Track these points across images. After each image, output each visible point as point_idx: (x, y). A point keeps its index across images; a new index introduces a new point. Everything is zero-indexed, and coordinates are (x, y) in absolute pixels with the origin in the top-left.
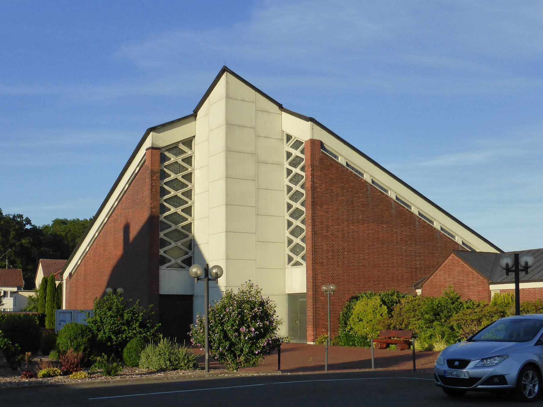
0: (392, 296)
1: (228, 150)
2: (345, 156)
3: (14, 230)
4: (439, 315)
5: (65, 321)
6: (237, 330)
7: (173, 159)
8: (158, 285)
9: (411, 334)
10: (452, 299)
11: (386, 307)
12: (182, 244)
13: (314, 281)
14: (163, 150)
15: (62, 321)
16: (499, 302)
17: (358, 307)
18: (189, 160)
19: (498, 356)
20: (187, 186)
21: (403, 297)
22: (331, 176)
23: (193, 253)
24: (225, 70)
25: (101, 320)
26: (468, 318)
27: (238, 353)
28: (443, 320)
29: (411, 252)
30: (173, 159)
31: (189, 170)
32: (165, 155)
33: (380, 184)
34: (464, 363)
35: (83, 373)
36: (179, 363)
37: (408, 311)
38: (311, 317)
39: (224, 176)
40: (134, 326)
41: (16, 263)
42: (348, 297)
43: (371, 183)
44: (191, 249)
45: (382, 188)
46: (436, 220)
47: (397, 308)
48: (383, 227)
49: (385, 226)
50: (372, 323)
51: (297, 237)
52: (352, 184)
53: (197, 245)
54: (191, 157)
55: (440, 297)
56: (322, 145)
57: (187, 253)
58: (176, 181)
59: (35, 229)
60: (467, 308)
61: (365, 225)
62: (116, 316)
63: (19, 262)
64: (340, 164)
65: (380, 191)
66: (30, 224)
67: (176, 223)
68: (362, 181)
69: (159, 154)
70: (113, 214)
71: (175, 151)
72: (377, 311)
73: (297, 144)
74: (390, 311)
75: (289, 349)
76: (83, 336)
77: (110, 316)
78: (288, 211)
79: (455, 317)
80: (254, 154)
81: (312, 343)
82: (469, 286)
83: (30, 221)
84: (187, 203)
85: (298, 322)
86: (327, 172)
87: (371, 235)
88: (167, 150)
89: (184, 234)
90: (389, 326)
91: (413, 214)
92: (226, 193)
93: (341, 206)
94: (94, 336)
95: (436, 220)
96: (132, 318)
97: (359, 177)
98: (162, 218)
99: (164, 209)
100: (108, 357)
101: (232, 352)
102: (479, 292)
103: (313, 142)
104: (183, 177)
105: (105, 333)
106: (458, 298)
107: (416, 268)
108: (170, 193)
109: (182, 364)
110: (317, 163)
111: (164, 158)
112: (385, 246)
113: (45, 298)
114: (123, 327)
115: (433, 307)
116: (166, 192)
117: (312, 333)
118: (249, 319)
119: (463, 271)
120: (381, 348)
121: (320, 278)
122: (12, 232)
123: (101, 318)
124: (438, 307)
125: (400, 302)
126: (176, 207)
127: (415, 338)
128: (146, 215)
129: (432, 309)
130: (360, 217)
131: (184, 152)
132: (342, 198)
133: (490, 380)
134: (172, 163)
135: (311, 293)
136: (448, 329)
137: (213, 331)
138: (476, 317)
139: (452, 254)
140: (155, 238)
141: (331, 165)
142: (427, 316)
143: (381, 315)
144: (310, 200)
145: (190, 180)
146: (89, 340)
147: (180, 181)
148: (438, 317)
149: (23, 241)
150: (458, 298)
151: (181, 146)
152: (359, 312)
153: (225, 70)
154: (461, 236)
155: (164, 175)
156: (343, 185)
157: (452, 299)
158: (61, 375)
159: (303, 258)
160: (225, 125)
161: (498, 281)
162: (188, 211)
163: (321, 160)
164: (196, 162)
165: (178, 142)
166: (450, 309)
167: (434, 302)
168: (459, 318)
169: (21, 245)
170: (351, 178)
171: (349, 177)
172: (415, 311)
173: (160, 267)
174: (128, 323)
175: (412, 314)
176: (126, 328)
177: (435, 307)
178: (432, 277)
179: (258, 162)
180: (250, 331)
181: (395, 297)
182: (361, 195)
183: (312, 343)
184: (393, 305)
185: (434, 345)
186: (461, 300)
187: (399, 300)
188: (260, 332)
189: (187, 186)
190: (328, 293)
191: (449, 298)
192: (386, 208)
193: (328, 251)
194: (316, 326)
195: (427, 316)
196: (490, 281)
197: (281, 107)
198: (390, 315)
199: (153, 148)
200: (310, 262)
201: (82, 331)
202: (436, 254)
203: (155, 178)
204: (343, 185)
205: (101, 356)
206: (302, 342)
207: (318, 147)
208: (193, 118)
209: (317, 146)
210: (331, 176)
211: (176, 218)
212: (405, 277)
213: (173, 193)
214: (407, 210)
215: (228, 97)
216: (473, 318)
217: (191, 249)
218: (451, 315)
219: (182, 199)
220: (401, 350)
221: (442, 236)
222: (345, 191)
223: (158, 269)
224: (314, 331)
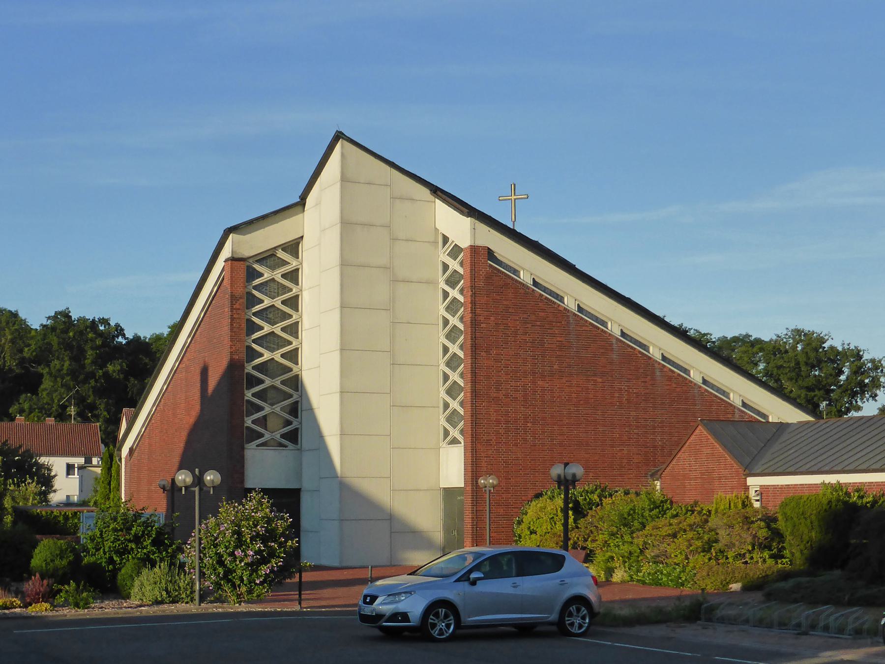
1: (344, 264)
2: (529, 268)
3: (92, 348)
6: (232, 554)
7: (267, 274)
8: (243, 474)
12: (282, 409)
13: (474, 469)
17: (533, 509)
18: (293, 276)
19: (404, 593)
20: (290, 316)
21: (611, 495)
23: (301, 423)
24: (339, 136)
25: (101, 535)
27: (238, 582)
31: (294, 291)
33: (593, 312)
34: (374, 598)
35: (46, 605)
36: (180, 594)
40: (145, 543)
41: (97, 409)
42: (531, 493)
44: (296, 417)
49: (600, 380)
51: (454, 400)
53: (311, 409)
54: (298, 270)
56: (490, 254)
57: (289, 423)
58: (272, 310)
59: (136, 341)
61: (564, 380)
62: (121, 530)
63: (102, 407)
66: (124, 335)
69: (244, 268)
70: (185, 359)
71: (270, 262)
73: (455, 251)
76: (62, 558)
77: (113, 529)
78: (444, 356)
83: (122, 330)
84: (290, 343)
86: (498, 297)
89: (285, 393)
93: (525, 347)
94: (78, 559)
96: (143, 532)
97: (554, 303)
98: (249, 368)
100: (78, 585)
101: (229, 581)
103: (474, 250)
104: (283, 302)
105: (105, 553)
107: (655, 447)
108: (262, 328)
109: (184, 596)
110: (482, 284)
111: (253, 274)
112: (599, 412)
113: (109, 484)
114: (130, 544)
116: (255, 328)
118: (248, 541)
121: (484, 464)
122: (90, 352)
123: (102, 532)
126: (272, 350)
128: (224, 363)
131: (285, 263)
132: (523, 337)
133: (394, 617)
134: (266, 282)
135: (469, 488)
137: (205, 555)
140: (249, 399)
141: (506, 285)
144: (469, 342)
146: (70, 563)
147: (278, 309)
149: (110, 368)
151: (281, 254)
153: (339, 136)
155: (253, 301)
156: (525, 316)
158: (20, 607)
159: (462, 432)
160: (338, 226)
164: (305, 277)
165: (275, 248)
169: (106, 375)
170: (541, 304)
171: (540, 305)
173: (246, 446)
174: (137, 539)
176: (133, 546)
178: (674, 462)
180: (246, 555)
181: (595, 498)
188: (262, 556)
189: (290, 316)
192: (602, 351)
193: (498, 422)
199: (233, 260)
201: (61, 551)
205: (69, 584)
208: (300, 208)
212: (636, 461)
213: (267, 328)
215: (345, 179)
221: (703, 393)
222: (529, 326)
223: (243, 449)
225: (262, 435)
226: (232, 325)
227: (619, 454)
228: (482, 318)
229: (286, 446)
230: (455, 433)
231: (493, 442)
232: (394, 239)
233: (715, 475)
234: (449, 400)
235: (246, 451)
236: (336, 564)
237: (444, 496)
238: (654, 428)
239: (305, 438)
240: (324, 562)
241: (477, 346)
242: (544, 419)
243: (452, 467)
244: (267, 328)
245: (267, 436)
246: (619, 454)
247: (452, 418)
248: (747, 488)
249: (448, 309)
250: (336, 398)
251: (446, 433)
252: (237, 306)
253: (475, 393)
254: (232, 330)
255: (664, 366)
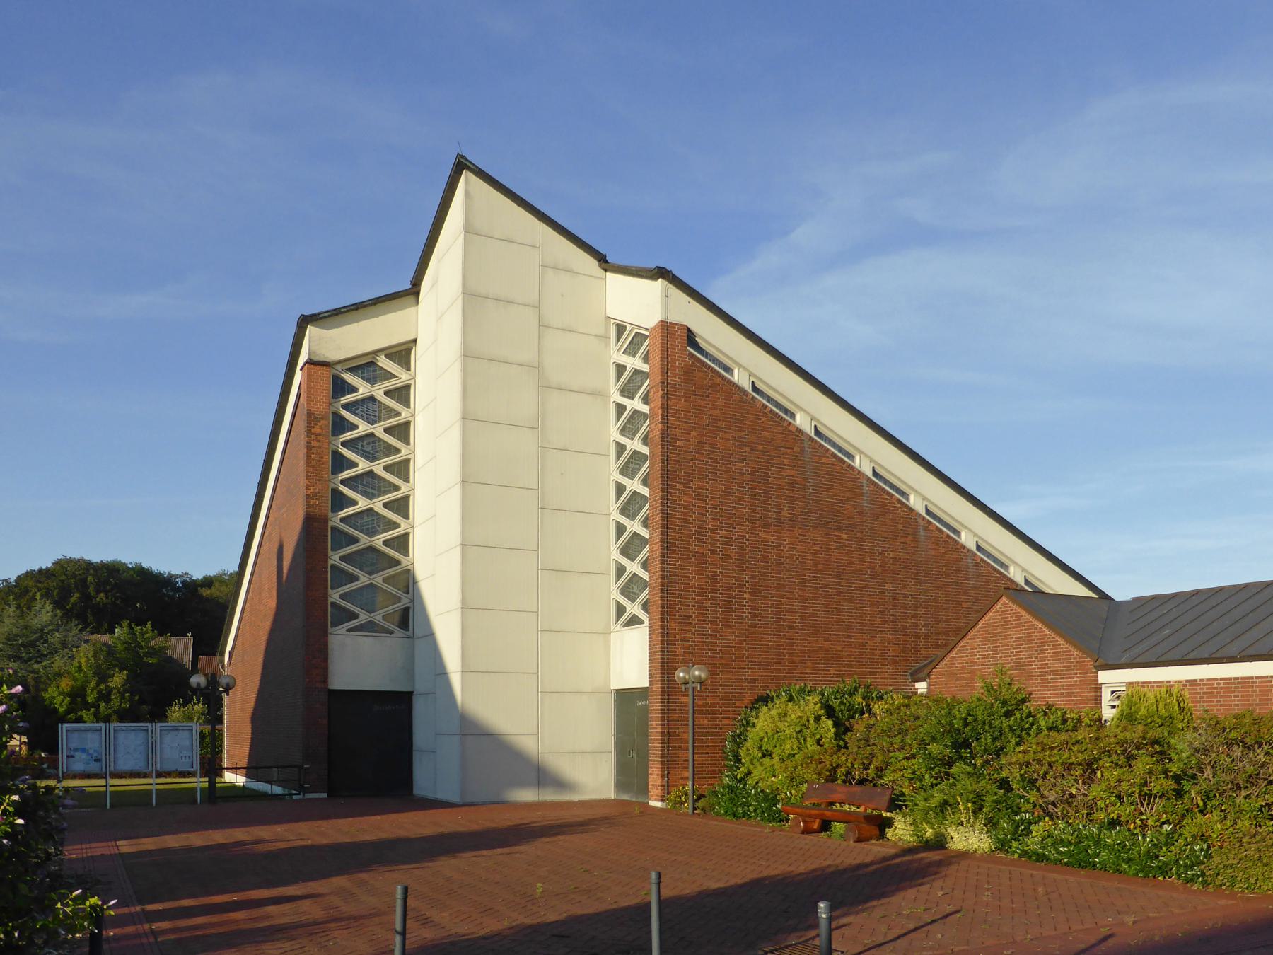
0: (851, 694)
1: (468, 355)
2: (748, 367)
4: (968, 746)
5: (83, 750)
7: (364, 389)
8: (326, 669)
9: (886, 799)
10: (1004, 703)
11: (830, 723)
12: (385, 580)
13: (665, 658)
14: (339, 367)
15: (76, 750)
16: (1143, 712)
17: (764, 721)
18: (402, 394)
21: (881, 698)
22: (712, 412)
23: (413, 601)
24: (461, 165)
26: (1056, 757)
28: (979, 762)
29: (906, 597)
30: (364, 389)
32: (343, 381)
37: (888, 733)
38: (657, 744)
39: (459, 415)
42: (749, 697)
43: (813, 434)
45: (840, 449)
46: (966, 527)
47: (860, 724)
48: (839, 538)
49: (845, 536)
50: (790, 764)
51: (633, 560)
52: (765, 434)
55: (972, 693)
56: (691, 338)
58: (371, 440)
60: (1050, 729)
61: (796, 533)
64: (735, 385)
65: (834, 455)
67: (371, 533)
68: (791, 428)
72: (806, 732)
74: (842, 729)
75: (551, 827)
79: (1014, 755)
80: (534, 367)
81: (658, 804)
82: (1043, 674)
84: (397, 488)
85: (634, 754)
86: (702, 403)
87: (810, 556)
88: (349, 370)
90: (834, 770)
91: (911, 510)
92: (463, 455)
95: (966, 527)
99: (340, 501)
102: (1069, 688)
104: (387, 430)
106: (1023, 701)
107: (917, 634)
110: (677, 381)
115: (951, 724)
117: (659, 781)
119: (1030, 639)
120: (807, 831)
121: (679, 652)
124: (966, 725)
125: (870, 711)
127: (900, 807)
129: (950, 729)
130: (785, 513)
134: (363, 400)
135: (657, 688)
136: (994, 788)
138: (1081, 757)
139: (1004, 599)
141: (714, 385)
142: (934, 748)
143: (818, 742)
145: (406, 440)
147: (380, 440)
148: (965, 753)
150: (1023, 701)
151: (383, 362)
152: (762, 734)
153: (461, 165)
154: (1023, 566)
156: (742, 434)
157: (1004, 703)
159: (645, 606)
161: (1123, 660)
162: (402, 506)
163: (688, 373)
164: (419, 396)
165: (376, 353)
166: (1001, 730)
167: (955, 712)
168: (1030, 757)
170: (763, 419)
171: (759, 420)
172: (903, 733)
173: (330, 630)
175: (898, 740)
177: (958, 724)
178: (953, 654)
179: (546, 387)
182: (786, 461)
183: (658, 804)
184: (853, 717)
185: (952, 831)
186: (1031, 706)
187: (868, 705)
190: (690, 686)
191: (997, 699)
192: (849, 494)
194: (669, 764)
195: (934, 748)
196: (1101, 661)
197: (602, 259)
198: (842, 743)
199: (310, 362)
200: (657, 614)
202: (965, 605)
203: (318, 431)
204: (742, 434)
206: (641, 800)
207: (681, 341)
208: (411, 299)
209: (677, 338)
210: (712, 412)
211: (369, 521)
212: (891, 653)
214: (899, 500)
215: (469, 229)
216: (1073, 760)
217: (408, 592)
218: (1002, 748)
219: (384, 480)
220: (859, 840)
221: (978, 564)
222: (747, 449)
223: (326, 634)
224: (663, 776)
225: (356, 616)
226: (308, 456)
227: (870, 643)
228: (678, 433)
229: (391, 633)
230: (634, 608)
231: (694, 619)
232: (544, 326)
233: (1035, 669)
234: (624, 561)
235: (330, 637)
236: (456, 799)
237: (616, 701)
238: (916, 608)
239: (415, 620)
240: (441, 795)
241: (669, 475)
242: (767, 588)
243: (630, 659)
244: (363, 465)
245: (363, 617)
246: (870, 643)
247: (628, 591)
248: (1098, 688)
249: (623, 431)
250: (456, 554)
251: (621, 610)
252: (316, 430)
253: (667, 545)
254: (308, 463)
255: (929, 522)
